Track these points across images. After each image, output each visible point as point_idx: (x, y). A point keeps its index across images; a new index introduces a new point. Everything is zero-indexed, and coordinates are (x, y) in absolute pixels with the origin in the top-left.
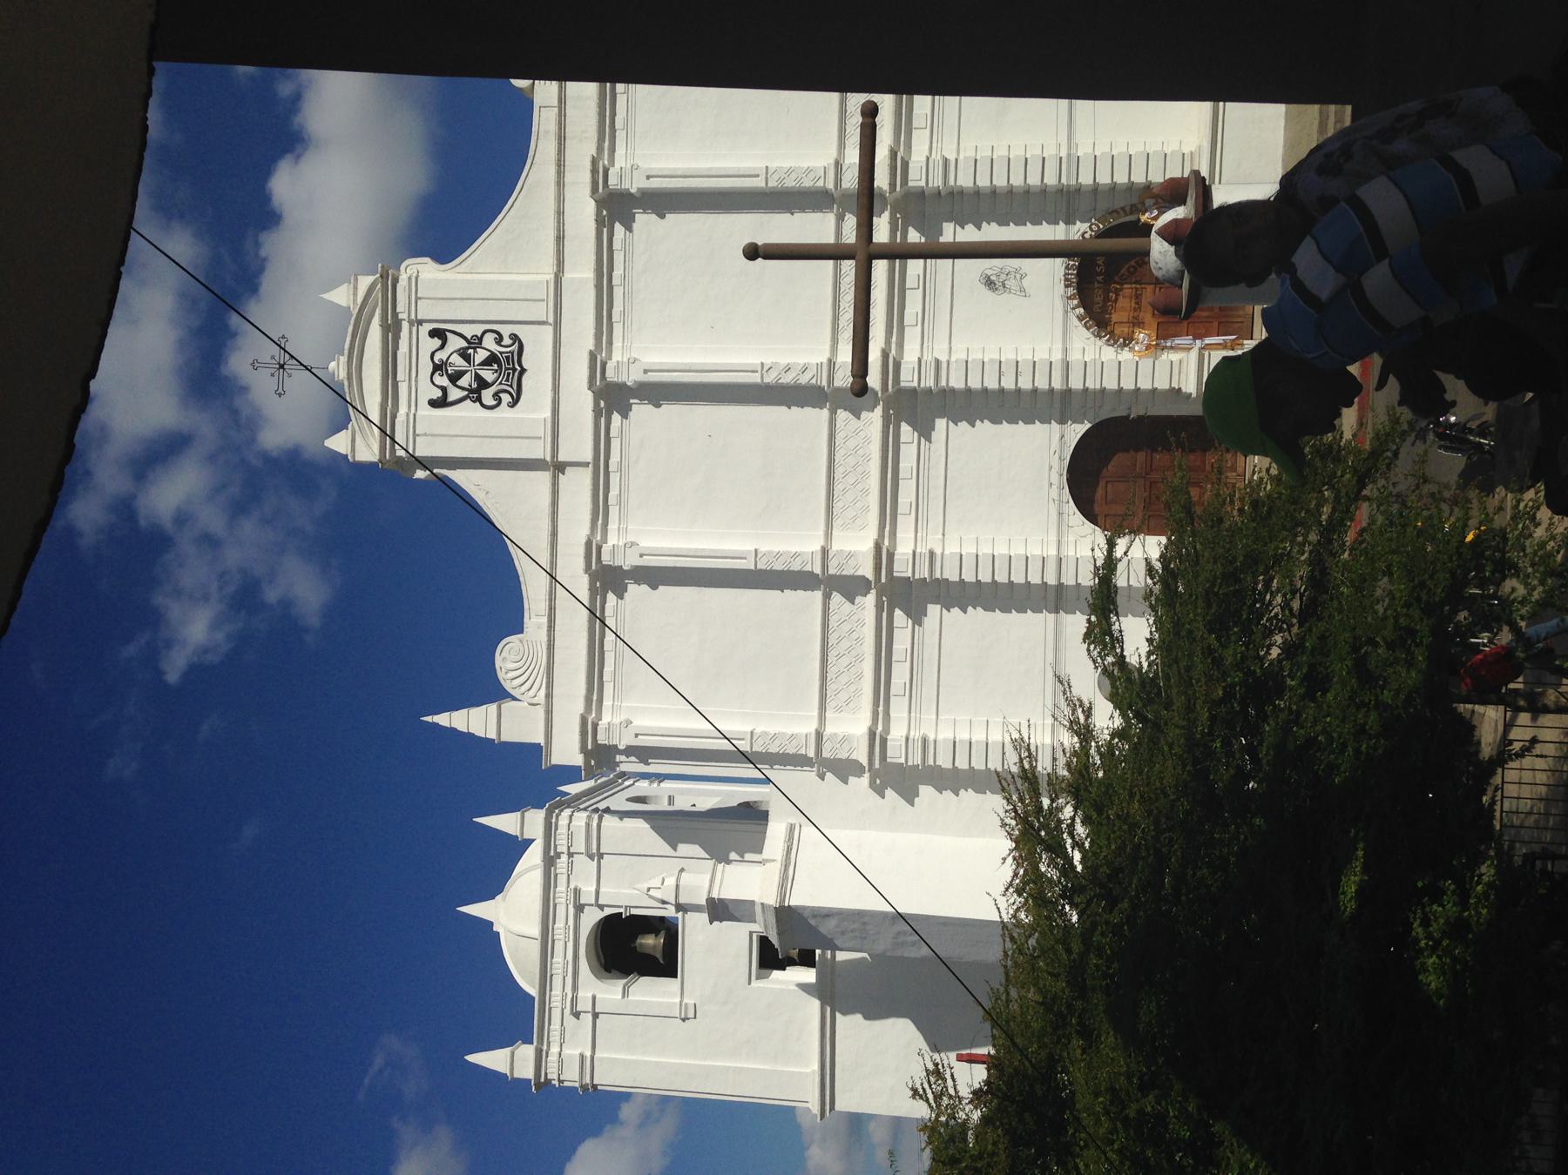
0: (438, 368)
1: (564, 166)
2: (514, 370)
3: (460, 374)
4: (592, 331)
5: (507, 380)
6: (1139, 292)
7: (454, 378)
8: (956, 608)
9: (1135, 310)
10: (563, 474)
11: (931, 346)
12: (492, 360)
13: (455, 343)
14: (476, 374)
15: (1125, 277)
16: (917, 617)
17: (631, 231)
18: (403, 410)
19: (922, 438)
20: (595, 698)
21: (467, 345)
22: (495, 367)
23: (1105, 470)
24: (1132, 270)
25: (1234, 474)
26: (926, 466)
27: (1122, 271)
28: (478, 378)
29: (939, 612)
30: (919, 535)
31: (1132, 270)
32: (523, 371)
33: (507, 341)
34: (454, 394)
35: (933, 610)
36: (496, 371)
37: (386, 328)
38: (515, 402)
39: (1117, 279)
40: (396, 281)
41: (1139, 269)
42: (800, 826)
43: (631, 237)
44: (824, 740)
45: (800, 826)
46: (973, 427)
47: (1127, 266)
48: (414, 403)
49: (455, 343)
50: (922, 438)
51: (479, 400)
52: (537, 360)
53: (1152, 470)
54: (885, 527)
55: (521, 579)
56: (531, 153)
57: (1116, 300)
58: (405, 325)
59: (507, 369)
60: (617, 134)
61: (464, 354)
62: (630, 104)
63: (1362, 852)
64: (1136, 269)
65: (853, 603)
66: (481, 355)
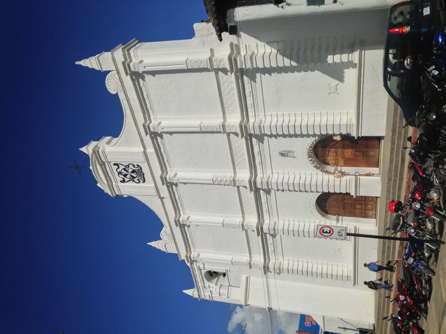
0: (120, 173)
1: (136, 120)
2: (141, 174)
3: (127, 175)
4: (159, 168)
5: (140, 176)
6: (336, 151)
7: (125, 176)
8: (267, 74)
9: (336, 156)
10: (164, 199)
11: (266, 171)
12: (133, 171)
13: (122, 167)
14: (131, 175)
15: (331, 147)
16: (253, 79)
17: (163, 139)
18: (114, 184)
19: (252, 81)
20: (188, 249)
21: (125, 167)
22: (135, 173)
23: (329, 199)
24: (333, 145)
25: (373, 202)
26: (270, 201)
27: (330, 145)
28: (131, 176)
29: (267, 139)
30: (271, 218)
31: (333, 145)
32: (143, 174)
33: (136, 166)
34: (126, 180)
35: (258, 75)
36: (136, 174)
37: (101, 165)
38: (144, 182)
39: (328, 147)
40: (98, 152)
41: (336, 144)
42: (250, 277)
43: (146, 83)
44: (244, 226)
45: (250, 277)
46: (277, 139)
47: (332, 143)
48: (116, 182)
49: (122, 167)
50: (252, 81)
51: (134, 181)
52: (145, 170)
53: (344, 200)
54: (260, 216)
55: (161, 220)
56: (124, 114)
57: (329, 153)
58: (106, 163)
59: (139, 174)
60: (149, 111)
61: (124, 169)
62: (164, 148)
63: (422, 228)
64: (335, 145)
65: (238, 137)
66: (130, 170)
